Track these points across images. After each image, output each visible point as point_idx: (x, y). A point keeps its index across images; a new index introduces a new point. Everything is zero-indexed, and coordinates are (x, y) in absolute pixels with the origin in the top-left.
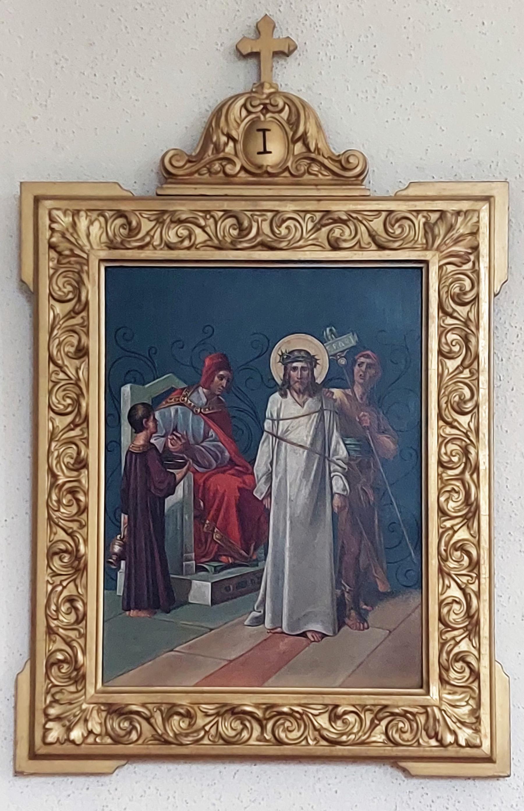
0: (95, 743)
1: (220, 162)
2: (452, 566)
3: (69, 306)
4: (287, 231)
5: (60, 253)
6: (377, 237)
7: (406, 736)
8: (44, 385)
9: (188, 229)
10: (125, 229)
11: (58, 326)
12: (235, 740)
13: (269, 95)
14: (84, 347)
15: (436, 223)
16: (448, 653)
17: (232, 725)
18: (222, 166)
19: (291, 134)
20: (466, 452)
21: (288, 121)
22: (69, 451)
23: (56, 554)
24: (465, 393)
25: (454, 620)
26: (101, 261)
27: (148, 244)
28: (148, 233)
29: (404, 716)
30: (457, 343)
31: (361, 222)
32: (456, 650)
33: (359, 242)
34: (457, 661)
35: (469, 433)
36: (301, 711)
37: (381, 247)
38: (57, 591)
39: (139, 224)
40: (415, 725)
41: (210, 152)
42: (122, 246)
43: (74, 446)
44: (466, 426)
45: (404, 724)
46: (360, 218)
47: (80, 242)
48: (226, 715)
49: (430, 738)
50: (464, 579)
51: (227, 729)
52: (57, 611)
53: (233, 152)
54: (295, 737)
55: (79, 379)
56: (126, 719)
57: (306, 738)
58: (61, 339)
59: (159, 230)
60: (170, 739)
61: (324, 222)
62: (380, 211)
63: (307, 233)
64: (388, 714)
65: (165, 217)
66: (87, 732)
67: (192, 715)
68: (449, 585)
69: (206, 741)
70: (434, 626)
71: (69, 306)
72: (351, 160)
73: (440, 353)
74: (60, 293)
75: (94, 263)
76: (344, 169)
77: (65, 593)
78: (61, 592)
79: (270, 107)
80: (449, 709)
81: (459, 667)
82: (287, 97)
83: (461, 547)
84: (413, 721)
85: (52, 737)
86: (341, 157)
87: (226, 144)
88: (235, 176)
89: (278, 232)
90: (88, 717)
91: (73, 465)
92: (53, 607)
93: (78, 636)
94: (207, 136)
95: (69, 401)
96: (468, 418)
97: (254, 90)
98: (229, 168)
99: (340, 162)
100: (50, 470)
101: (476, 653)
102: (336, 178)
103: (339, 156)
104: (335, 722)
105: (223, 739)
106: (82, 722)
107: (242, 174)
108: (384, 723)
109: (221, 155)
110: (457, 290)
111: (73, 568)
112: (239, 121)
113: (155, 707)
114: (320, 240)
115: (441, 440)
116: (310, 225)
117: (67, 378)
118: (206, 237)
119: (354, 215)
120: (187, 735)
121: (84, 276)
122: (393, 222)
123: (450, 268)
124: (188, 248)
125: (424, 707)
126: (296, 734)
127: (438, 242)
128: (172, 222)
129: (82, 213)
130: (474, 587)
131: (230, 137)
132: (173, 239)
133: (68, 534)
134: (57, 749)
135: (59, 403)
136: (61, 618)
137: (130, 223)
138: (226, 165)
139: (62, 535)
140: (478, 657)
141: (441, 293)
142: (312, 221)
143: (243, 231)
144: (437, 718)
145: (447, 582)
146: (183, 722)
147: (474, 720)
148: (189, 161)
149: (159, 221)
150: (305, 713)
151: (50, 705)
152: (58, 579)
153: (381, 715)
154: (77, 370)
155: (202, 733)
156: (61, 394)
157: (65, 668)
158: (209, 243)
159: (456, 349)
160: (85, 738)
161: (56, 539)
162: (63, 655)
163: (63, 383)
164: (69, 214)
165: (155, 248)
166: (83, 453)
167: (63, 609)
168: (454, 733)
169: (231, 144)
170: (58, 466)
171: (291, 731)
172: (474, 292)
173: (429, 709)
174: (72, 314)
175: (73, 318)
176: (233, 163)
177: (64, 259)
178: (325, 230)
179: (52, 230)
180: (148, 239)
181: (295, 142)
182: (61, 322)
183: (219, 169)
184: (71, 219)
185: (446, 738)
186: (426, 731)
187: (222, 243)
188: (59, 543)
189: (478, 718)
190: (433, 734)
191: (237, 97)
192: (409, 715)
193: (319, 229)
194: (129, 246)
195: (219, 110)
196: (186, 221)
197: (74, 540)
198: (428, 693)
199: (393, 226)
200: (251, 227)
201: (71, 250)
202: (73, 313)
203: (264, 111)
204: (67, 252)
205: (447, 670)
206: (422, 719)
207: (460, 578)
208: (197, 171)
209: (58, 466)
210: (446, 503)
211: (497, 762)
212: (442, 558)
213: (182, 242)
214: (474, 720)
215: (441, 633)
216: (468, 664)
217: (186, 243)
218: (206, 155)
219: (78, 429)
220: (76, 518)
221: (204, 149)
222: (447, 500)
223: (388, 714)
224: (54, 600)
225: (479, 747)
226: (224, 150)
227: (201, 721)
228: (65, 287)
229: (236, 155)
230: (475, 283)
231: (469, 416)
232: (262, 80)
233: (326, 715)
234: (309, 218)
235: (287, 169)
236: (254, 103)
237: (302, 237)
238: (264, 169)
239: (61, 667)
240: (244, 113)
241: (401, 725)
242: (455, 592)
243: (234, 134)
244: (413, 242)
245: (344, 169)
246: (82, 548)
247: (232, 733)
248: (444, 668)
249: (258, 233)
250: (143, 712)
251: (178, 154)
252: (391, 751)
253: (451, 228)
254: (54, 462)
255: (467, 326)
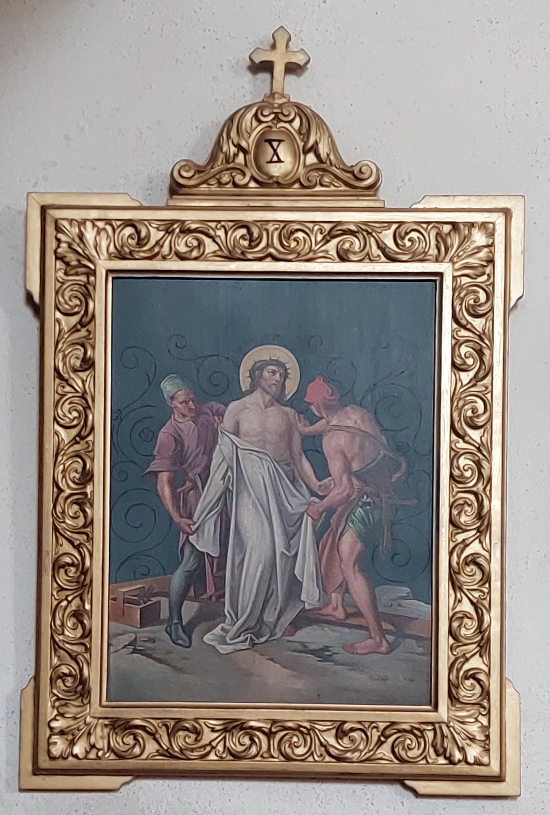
0: (98, 758)
1: (229, 172)
2: (464, 580)
3: (74, 320)
4: (295, 243)
5: (67, 264)
6: (387, 250)
7: (411, 754)
8: (50, 399)
9: (197, 239)
10: (133, 239)
11: (64, 340)
12: (244, 754)
13: (280, 106)
14: (90, 359)
15: (449, 234)
16: (458, 671)
17: (241, 740)
18: (232, 176)
19: (301, 144)
20: (480, 353)
21: (299, 132)
22: (75, 465)
23: (63, 567)
24: (478, 407)
25: (465, 635)
26: (109, 271)
27: (157, 254)
28: (157, 243)
29: (411, 732)
30: (470, 354)
31: (371, 234)
32: (466, 667)
33: (368, 254)
34: (467, 678)
35: (481, 448)
36: (309, 727)
37: (392, 260)
38: (62, 606)
39: (148, 236)
40: (422, 741)
41: (219, 163)
42: (130, 256)
43: (80, 460)
44: (479, 442)
45: (299, 740)
46: (370, 231)
47: (87, 252)
48: (233, 730)
49: (438, 755)
50: (477, 594)
51: (235, 745)
52: (63, 625)
53: (243, 162)
54: (302, 753)
55: (85, 392)
56: (246, 734)
57: (425, 758)
58: (67, 352)
59: (170, 238)
60: (176, 754)
61: (334, 233)
62: (391, 223)
63: (316, 244)
64: (395, 731)
65: (175, 226)
66: (90, 747)
67: (198, 731)
68: (460, 599)
69: (212, 757)
70: (444, 640)
71: (74, 320)
72: (363, 169)
73: (454, 364)
74: (67, 307)
75: (101, 273)
76: (358, 179)
77: (332, 741)
78: (65, 609)
79: (281, 116)
80: (457, 726)
81: (469, 685)
82: (298, 106)
83: (473, 560)
84: (421, 737)
85: (56, 751)
86: (354, 168)
87: (236, 155)
88: (246, 186)
89: (285, 243)
90: (92, 731)
91: (79, 479)
92: (58, 622)
93: (83, 651)
94: (218, 146)
95: (75, 414)
96: (483, 320)
97: (265, 100)
98: (239, 179)
99: (352, 173)
100: (55, 483)
101: (486, 669)
102: (348, 189)
103: (352, 166)
104: (342, 739)
105: (231, 754)
106: (85, 736)
107: (252, 184)
108: (391, 740)
109: (231, 165)
110: (472, 302)
111: (78, 582)
112: (249, 131)
113: (160, 723)
114: (330, 253)
115: (453, 453)
116: (320, 237)
117: (73, 391)
118: (216, 248)
119: (363, 227)
120: (192, 750)
121: (91, 288)
122: (403, 234)
123: (465, 280)
124: (196, 259)
125: (432, 724)
126: (300, 751)
127: (451, 253)
128: (182, 231)
129: (89, 224)
130: (486, 603)
131: (240, 148)
132: (182, 249)
133: (74, 547)
134: (60, 764)
135: (66, 303)
136: (66, 633)
137: (138, 232)
138: (235, 175)
139: (67, 547)
140: (488, 557)
141: (455, 304)
142: (321, 233)
143: (253, 242)
144: (445, 735)
145: (459, 595)
146: (189, 737)
147: (484, 738)
148: (199, 172)
149: (169, 232)
150: (313, 729)
151: (55, 719)
152: (64, 594)
153: (387, 732)
154: (83, 382)
155: (208, 749)
156: (67, 406)
157: (69, 681)
158: (219, 253)
159: (470, 361)
160: (87, 752)
161: (60, 553)
162: (68, 669)
163: (70, 395)
164: (75, 225)
165: (164, 258)
166: (88, 467)
167: (69, 624)
168: (462, 750)
169: (241, 155)
170: (64, 480)
171: (297, 747)
172: (489, 304)
173: (437, 726)
174: (78, 439)
175: (78, 331)
176: (244, 174)
177: (72, 269)
178: (335, 241)
179: (59, 241)
180: (156, 250)
181: (306, 152)
182: (66, 336)
183: (228, 180)
184: (77, 230)
185: (454, 756)
186: (434, 746)
187: (232, 253)
188: (64, 556)
189: (488, 737)
190: (441, 751)
191: (248, 108)
192: (416, 731)
193: (328, 241)
194: (137, 257)
195: (231, 119)
196: (196, 231)
197: (80, 553)
198: (436, 709)
199: (403, 238)
200: (260, 237)
201: (79, 261)
202: (82, 324)
203: (275, 122)
204: (74, 263)
205: (457, 687)
206: (430, 735)
207: (473, 593)
208: (205, 182)
209: (64, 480)
210: (458, 516)
211: (507, 779)
212: (454, 571)
213: (191, 251)
214: (484, 738)
215: (452, 648)
216: (479, 681)
217: (195, 254)
218: (216, 165)
219: (83, 442)
220: (83, 530)
221: (213, 158)
222: (459, 514)
223: (395, 731)
224: (58, 615)
225: (488, 765)
226: (233, 161)
227: (208, 736)
228: (71, 300)
229: (246, 165)
230: (489, 296)
231: (482, 430)
232: (274, 91)
233: (334, 731)
234: (318, 230)
235: (298, 181)
236: (265, 113)
237: (311, 250)
238: (275, 179)
239: (66, 680)
240: (255, 123)
241: (408, 742)
242: (466, 607)
243: (244, 144)
244: (423, 255)
245: (358, 179)
246: (88, 563)
247: (240, 748)
248: (453, 687)
249: (268, 246)
250: (148, 727)
251: (188, 165)
252: (397, 768)
253: (465, 239)
254: (60, 476)
255: (482, 340)
